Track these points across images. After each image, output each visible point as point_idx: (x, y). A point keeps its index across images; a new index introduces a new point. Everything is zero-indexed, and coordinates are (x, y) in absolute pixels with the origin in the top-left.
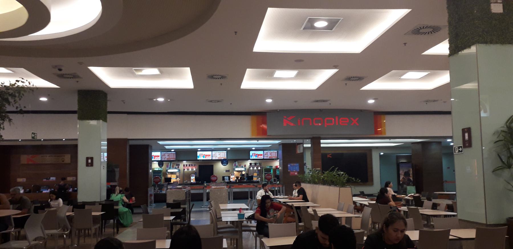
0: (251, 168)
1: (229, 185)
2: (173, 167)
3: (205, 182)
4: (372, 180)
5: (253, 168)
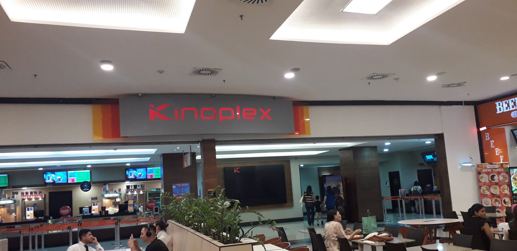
2: (5, 197)
3: (51, 217)
4: (292, 200)
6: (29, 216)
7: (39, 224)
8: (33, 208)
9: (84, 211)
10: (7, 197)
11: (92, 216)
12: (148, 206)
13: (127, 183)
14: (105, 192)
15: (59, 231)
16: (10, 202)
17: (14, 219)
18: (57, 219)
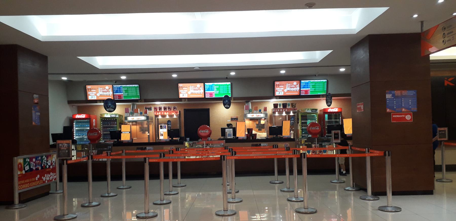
0: (277, 114)
1: (231, 146)
3: (188, 139)
5: (280, 113)
6: (162, 135)
7: (173, 147)
8: (166, 125)
9: (227, 132)
10: (139, 112)
11: (236, 140)
12: (311, 131)
13: (274, 101)
14: (248, 111)
15: (198, 157)
16: (143, 118)
17: (147, 139)
18: (194, 142)
